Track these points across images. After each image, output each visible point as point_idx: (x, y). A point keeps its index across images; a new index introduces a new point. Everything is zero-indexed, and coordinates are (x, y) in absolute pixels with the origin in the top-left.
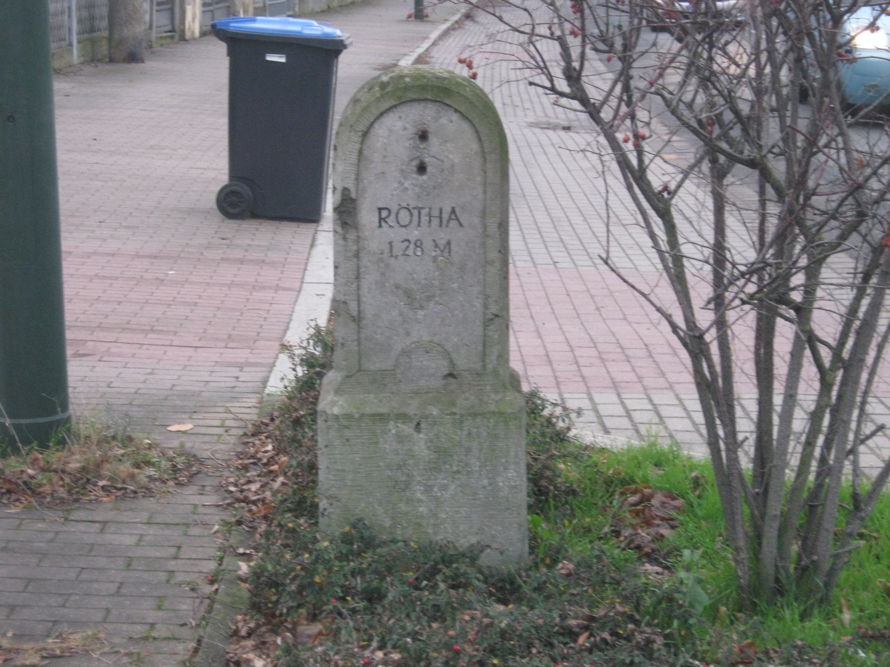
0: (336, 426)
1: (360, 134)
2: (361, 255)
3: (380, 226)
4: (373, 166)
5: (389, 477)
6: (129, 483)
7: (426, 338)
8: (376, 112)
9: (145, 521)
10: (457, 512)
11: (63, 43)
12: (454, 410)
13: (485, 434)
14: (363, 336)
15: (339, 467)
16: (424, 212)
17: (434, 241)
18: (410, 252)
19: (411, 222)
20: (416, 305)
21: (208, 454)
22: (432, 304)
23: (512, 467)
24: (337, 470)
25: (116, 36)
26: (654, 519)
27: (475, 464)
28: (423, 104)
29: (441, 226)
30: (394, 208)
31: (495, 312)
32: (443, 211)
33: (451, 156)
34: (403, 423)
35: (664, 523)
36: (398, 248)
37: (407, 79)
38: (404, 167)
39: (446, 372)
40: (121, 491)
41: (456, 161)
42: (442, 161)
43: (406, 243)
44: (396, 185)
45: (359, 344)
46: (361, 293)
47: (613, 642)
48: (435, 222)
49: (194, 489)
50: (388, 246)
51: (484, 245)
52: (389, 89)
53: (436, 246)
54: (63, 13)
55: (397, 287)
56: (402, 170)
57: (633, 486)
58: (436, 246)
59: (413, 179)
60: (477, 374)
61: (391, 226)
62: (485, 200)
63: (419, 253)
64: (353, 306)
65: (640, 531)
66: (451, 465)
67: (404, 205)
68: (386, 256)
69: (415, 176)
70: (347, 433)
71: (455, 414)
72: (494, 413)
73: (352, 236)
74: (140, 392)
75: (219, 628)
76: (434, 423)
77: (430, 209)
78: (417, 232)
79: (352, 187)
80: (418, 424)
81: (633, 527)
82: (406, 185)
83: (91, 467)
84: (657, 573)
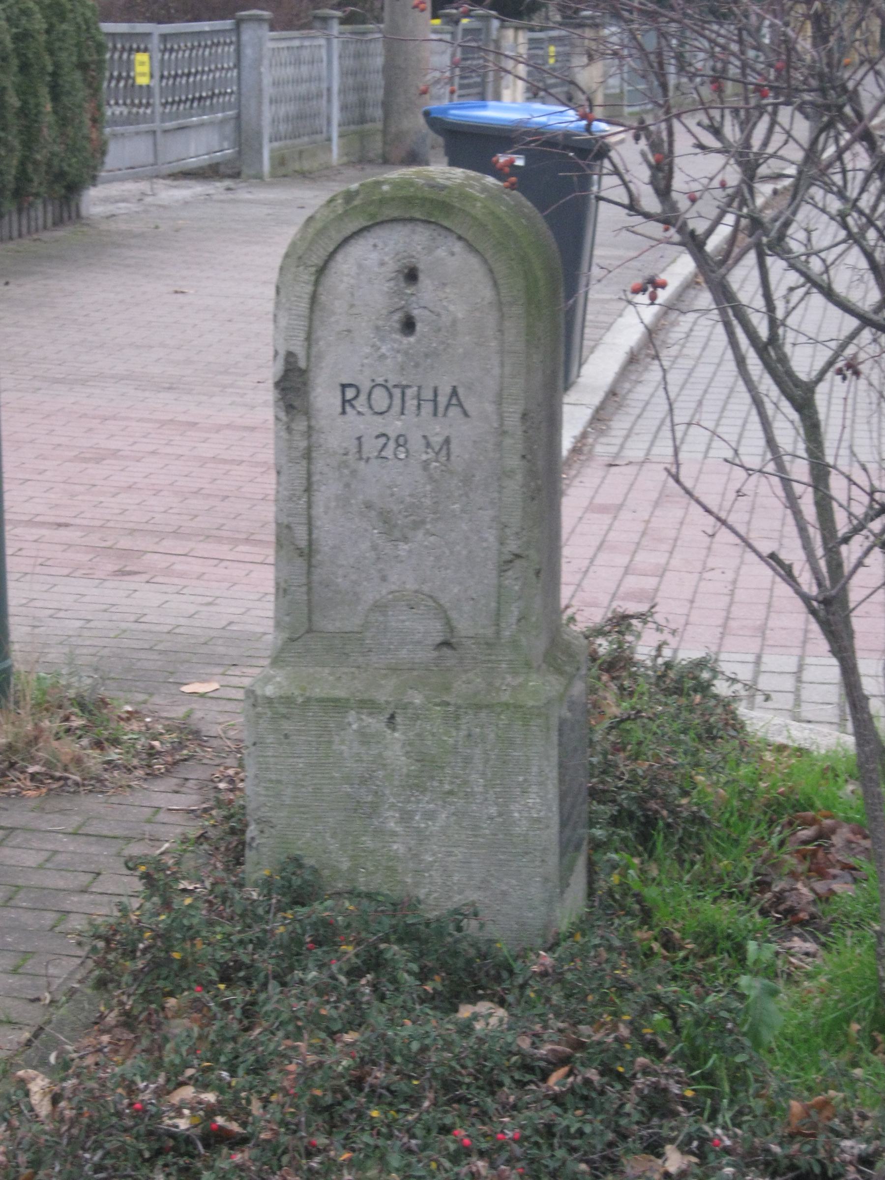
0: (269, 714)
1: (313, 269)
2: (314, 455)
3: (344, 412)
4: (333, 319)
5: (348, 795)
6: (73, 770)
7: (411, 586)
8: (337, 237)
9: (70, 830)
10: (450, 854)
11: (318, 137)
12: (446, 698)
13: (492, 736)
14: (315, 578)
15: (273, 777)
16: (410, 392)
17: (425, 437)
18: (388, 452)
19: (390, 407)
20: (397, 534)
21: (217, 730)
22: (420, 534)
23: (534, 789)
24: (271, 781)
25: (393, 129)
26: (833, 866)
27: (478, 783)
28: (409, 226)
29: (435, 414)
30: (365, 386)
31: (517, 551)
32: (440, 392)
33: (452, 308)
34: (370, 714)
35: (846, 874)
36: (371, 446)
37: (386, 188)
38: (380, 323)
39: (439, 640)
40: (56, 782)
41: (460, 315)
42: (438, 315)
43: (383, 440)
44: (368, 350)
45: (309, 592)
46: (314, 512)
47: (603, 1086)
48: (427, 408)
49: (171, 782)
50: (356, 442)
51: (499, 445)
52: (357, 202)
53: (428, 445)
54: (319, 96)
55: (369, 506)
56: (377, 328)
57: (811, 813)
58: (428, 445)
59: (394, 341)
60: (487, 644)
61: (359, 413)
62: (502, 376)
63: (402, 456)
64: (301, 532)
65: (799, 885)
66: (441, 782)
67: (380, 380)
68: (351, 457)
69: (397, 336)
70: (287, 726)
71: (448, 704)
72: (507, 705)
73: (300, 425)
74: (177, 631)
75: (83, 1009)
76: (416, 718)
77: (420, 387)
78: (399, 423)
79: (301, 352)
80: (392, 717)
81: (793, 875)
82: (384, 350)
83: (20, 745)
84: (807, 954)
